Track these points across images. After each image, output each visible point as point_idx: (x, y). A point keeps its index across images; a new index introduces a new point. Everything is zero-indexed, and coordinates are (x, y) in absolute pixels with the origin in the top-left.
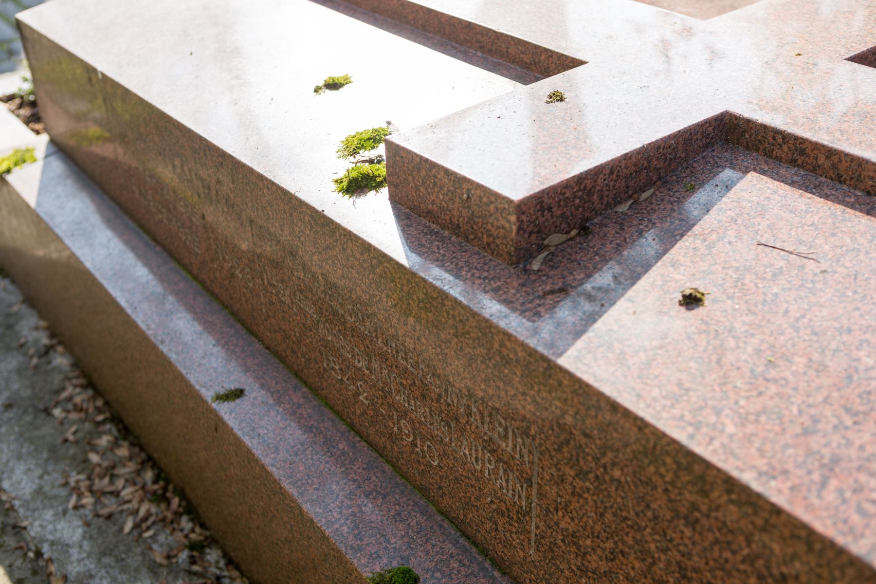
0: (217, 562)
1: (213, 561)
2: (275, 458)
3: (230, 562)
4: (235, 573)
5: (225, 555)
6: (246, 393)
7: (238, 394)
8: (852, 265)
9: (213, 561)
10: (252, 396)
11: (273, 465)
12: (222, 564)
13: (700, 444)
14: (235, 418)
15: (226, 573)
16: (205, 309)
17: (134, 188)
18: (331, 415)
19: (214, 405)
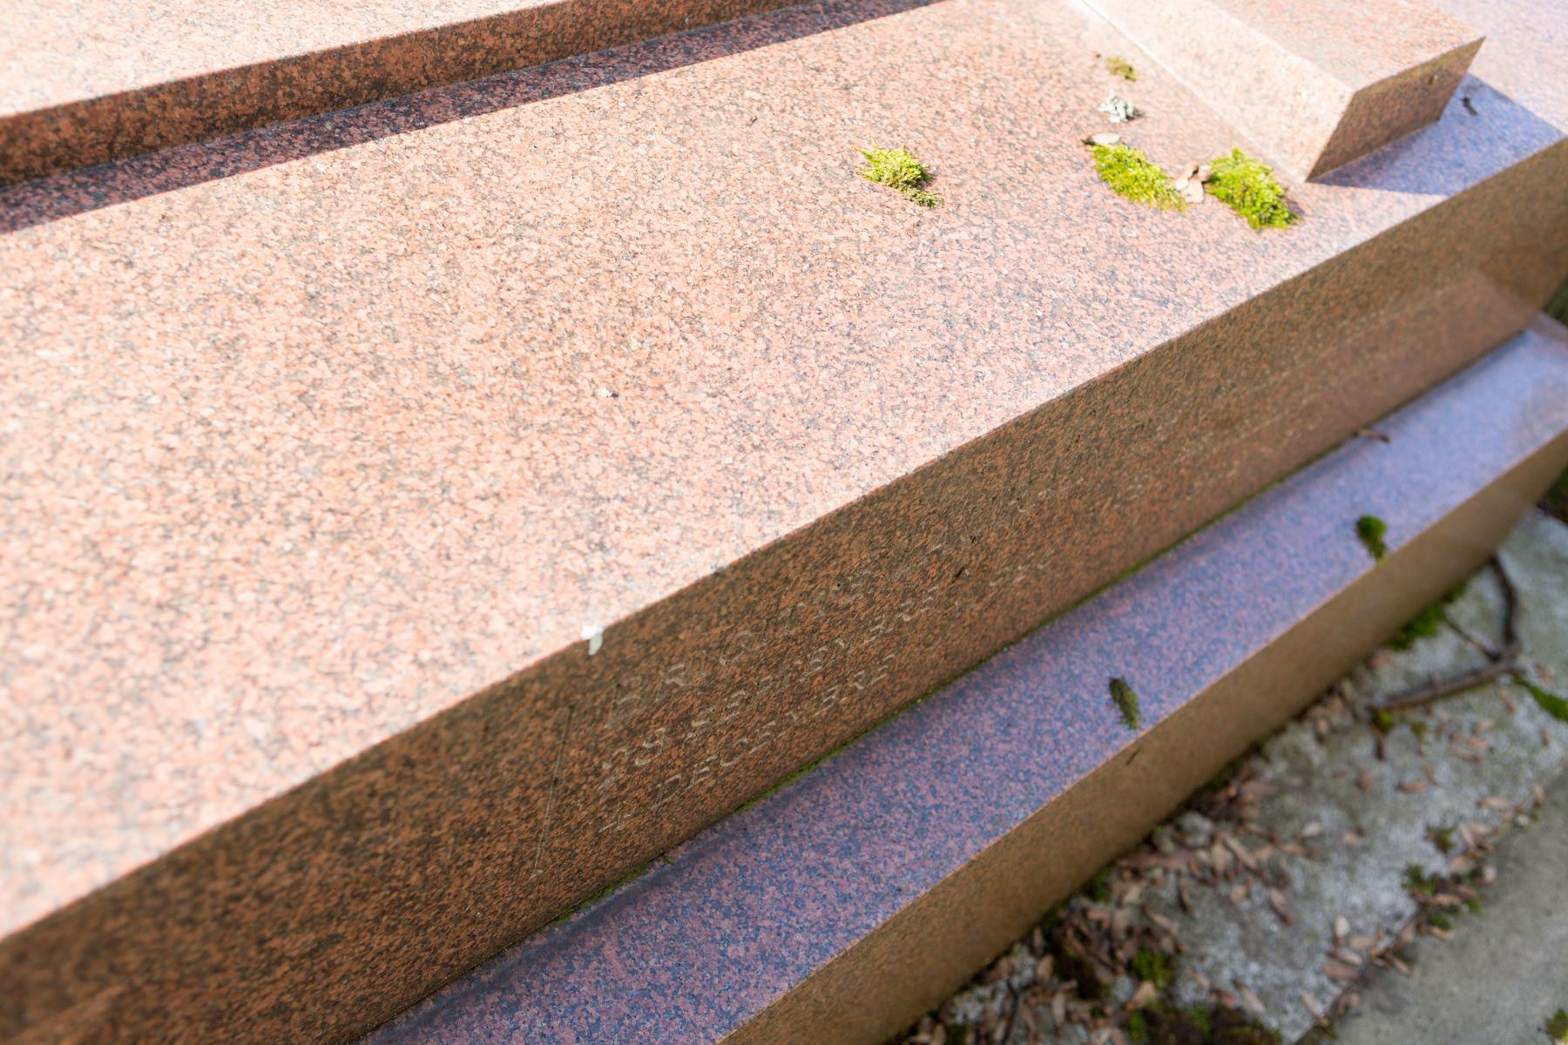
0: (981, 1000)
1: (979, 1007)
2: (1234, 645)
3: (979, 979)
4: (1004, 964)
5: (964, 988)
6: (1118, 676)
7: (1118, 690)
8: (301, 529)
9: (979, 1007)
10: (1123, 668)
11: (1245, 648)
12: (984, 991)
13: (122, 851)
14: (1169, 695)
15: (1002, 985)
16: (907, 742)
17: (1236, 463)
18: (1151, 566)
19: (1145, 728)
